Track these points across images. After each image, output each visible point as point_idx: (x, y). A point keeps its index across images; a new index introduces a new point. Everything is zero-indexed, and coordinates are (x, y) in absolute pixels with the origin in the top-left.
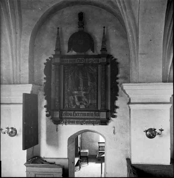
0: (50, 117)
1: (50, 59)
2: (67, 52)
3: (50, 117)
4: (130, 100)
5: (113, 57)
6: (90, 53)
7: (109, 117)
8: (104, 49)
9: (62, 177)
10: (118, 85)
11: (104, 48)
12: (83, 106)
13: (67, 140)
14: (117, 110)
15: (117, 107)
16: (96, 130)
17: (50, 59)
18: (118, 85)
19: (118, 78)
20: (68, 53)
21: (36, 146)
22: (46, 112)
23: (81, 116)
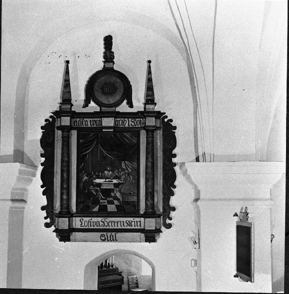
0: (53, 228)
1: (51, 120)
2: (82, 103)
3: (53, 228)
4: (198, 192)
5: (166, 117)
6: (124, 108)
7: (161, 228)
8: (150, 99)
9: (45, 211)
10: (175, 168)
11: (150, 100)
12: (113, 206)
13: (84, 268)
14: (172, 214)
15: (174, 209)
16: (140, 252)
17: (51, 120)
18: (175, 168)
19: (175, 156)
20: (83, 107)
21: (76, 134)
22: (126, 270)
23: (115, 226)
